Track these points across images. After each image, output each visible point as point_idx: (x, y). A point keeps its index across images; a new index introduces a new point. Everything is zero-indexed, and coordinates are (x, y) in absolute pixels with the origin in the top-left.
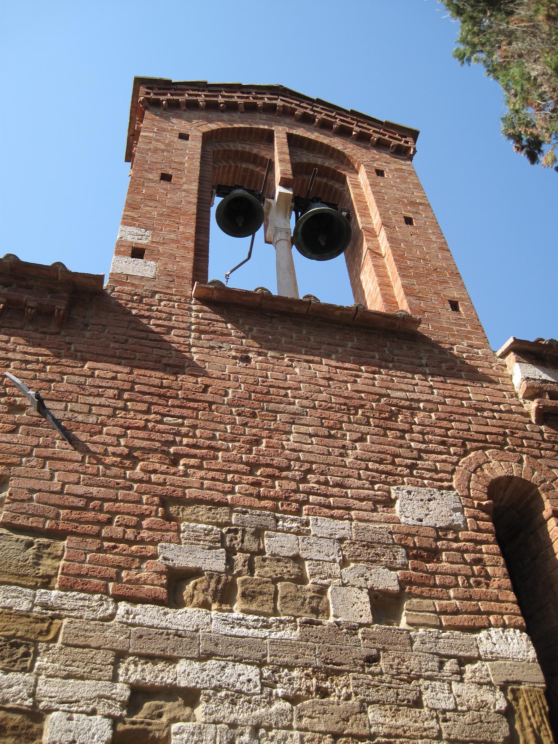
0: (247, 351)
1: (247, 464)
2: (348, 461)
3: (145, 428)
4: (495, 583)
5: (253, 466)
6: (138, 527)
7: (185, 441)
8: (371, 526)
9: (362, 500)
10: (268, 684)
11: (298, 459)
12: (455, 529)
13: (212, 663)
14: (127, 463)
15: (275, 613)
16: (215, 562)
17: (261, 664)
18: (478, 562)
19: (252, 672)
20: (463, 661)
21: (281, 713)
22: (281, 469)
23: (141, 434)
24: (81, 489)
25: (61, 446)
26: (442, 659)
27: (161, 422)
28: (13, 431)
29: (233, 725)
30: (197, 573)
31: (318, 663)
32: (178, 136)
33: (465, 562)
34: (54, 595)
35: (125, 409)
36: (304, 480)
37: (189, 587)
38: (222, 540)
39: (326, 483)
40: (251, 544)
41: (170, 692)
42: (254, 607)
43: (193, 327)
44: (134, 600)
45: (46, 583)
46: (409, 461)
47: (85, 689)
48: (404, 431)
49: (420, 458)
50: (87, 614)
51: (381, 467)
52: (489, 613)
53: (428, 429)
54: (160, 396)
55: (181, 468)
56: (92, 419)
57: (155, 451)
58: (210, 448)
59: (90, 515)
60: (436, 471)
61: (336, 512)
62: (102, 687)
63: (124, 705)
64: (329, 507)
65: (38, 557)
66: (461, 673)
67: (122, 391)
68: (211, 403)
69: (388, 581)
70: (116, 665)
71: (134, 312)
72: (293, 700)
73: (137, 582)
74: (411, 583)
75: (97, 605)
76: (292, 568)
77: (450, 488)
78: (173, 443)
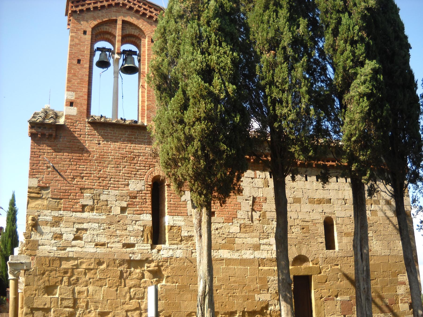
0: (100, 141)
1: (98, 177)
2: (121, 174)
3: (76, 170)
4: (147, 204)
5: (99, 178)
6: (76, 196)
7: (85, 172)
8: (123, 191)
9: (122, 185)
11: (109, 175)
12: (141, 191)
13: (90, 223)
14: (73, 180)
15: (102, 213)
16: (90, 203)
17: (99, 223)
18: (145, 199)
19: (97, 225)
20: (136, 221)
21: (102, 232)
22: (105, 178)
23: (75, 171)
24: (64, 188)
25: (59, 177)
26: (132, 221)
27: (79, 167)
28: (49, 174)
29: (93, 235)
30: (87, 205)
31: (109, 222)
32: (83, 32)
33: (142, 199)
34: (61, 212)
35: (71, 164)
36: (110, 180)
37: (86, 208)
38: (92, 198)
39: (115, 181)
40: (98, 198)
41: (83, 229)
42: (98, 212)
43: (87, 133)
44: (76, 212)
45: (60, 210)
46: (135, 173)
48: (135, 164)
49: (138, 171)
50: (68, 215)
51: (128, 175)
52: (144, 211)
53: (142, 162)
54: (79, 159)
55: (84, 180)
56: (65, 169)
57: (78, 176)
58: (90, 173)
59: (67, 194)
60: (141, 175)
61: (116, 189)
62: (72, 229)
63: (76, 232)
64: (115, 187)
65: (58, 204)
66: (135, 223)
67: (70, 159)
68: (90, 160)
69: (124, 204)
70: (74, 225)
71: (72, 130)
72: (104, 229)
73: (76, 208)
74: (129, 205)
76: (106, 203)
77: (143, 180)
78: (82, 173)
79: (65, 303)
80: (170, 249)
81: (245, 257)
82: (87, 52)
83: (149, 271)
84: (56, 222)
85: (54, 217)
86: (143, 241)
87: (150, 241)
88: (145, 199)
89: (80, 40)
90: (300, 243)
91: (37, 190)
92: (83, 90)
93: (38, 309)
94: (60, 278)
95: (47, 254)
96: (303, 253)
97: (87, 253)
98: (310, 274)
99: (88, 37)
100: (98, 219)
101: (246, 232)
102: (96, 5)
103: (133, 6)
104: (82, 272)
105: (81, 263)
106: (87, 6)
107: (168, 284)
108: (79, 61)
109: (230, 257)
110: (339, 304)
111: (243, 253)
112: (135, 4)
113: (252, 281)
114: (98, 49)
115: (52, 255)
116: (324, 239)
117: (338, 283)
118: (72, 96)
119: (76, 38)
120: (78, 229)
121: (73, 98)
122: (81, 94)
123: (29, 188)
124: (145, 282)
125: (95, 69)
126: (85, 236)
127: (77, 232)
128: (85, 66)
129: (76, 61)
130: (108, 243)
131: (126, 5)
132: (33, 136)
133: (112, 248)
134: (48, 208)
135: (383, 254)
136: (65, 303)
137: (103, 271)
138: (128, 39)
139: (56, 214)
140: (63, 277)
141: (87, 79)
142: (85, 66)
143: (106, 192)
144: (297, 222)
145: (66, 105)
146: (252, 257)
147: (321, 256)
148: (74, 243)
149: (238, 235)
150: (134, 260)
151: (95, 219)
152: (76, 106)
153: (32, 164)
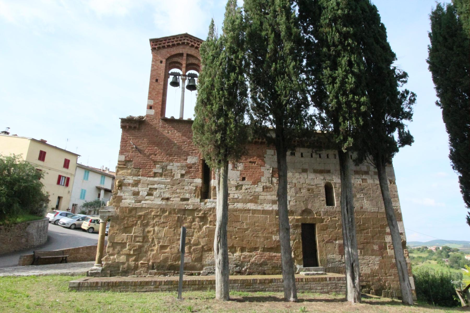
6: (150, 166)
10: (165, 187)
16: (160, 171)
19: (164, 186)
24: (143, 161)
34: (140, 177)
45: (139, 176)
47: (144, 189)
69: (183, 172)
75: (145, 178)
79: (138, 239)
80: (213, 202)
81: (266, 208)
82: (162, 75)
83: (198, 217)
84: (136, 184)
85: (135, 180)
86: (195, 196)
87: (200, 197)
88: (198, 168)
89: (158, 67)
90: (306, 200)
91: (124, 163)
92: (158, 97)
93: (117, 243)
94: (135, 222)
95: (127, 205)
96: (309, 207)
97: (157, 205)
98: (314, 223)
99: (163, 65)
100: (164, 182)
101: (267, 191)
102: (169, 44)
103: (193, 44)
104: (151, 217)
105: (152, 211)
106: (163, 45)
107: (211, 226)
108: (157, 80)
109: (255, 209)
110: (337, 246)
111: (264, 206)
112: (195, 43)
113: (270, 226)
114: (172, 74)
115: (131, 206)
116: (325, 198)
117: (337, 230)
118: (152, 102)
119: (155, 65)
120: (150, 188)
121: (152, 104)
122: (157, 101)
123: (119, 161)
124: (195, 225)
125: (186, 90)
126: (155, 193)
127: (149, 190)
128: (161, 83)
129: (154, 80)
130: (170, 198)
131: (189, 44)
132: (123, 127)
133: (173, 201)
134: (131, 175)
135: (372, 211)
136: (138, 239)
137: (166, 217)
138: (191, 66)
139: (136, 178)
140: (137, 221)
141: (162, 91)
142: (161, 83)
143: (171, 164)
144: (304, 185)
145: (147, 108)
146: (271, 209)
147: (323, 210)
148: (147, 197)
149: (261, 194)
150: (188, 210)
151: (163, 182)
152: (154, 109)
153: (122, 146)
